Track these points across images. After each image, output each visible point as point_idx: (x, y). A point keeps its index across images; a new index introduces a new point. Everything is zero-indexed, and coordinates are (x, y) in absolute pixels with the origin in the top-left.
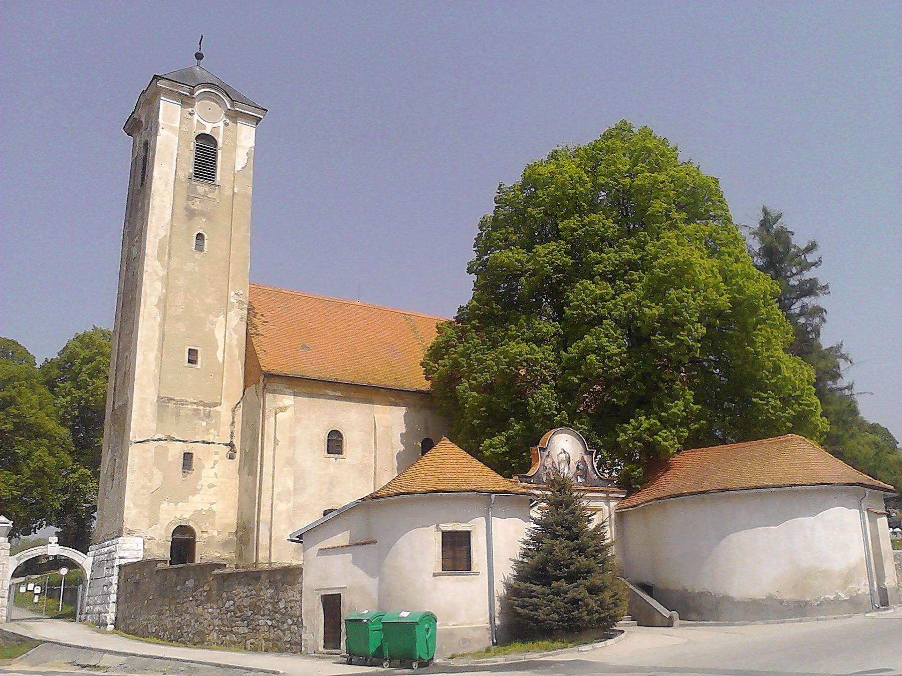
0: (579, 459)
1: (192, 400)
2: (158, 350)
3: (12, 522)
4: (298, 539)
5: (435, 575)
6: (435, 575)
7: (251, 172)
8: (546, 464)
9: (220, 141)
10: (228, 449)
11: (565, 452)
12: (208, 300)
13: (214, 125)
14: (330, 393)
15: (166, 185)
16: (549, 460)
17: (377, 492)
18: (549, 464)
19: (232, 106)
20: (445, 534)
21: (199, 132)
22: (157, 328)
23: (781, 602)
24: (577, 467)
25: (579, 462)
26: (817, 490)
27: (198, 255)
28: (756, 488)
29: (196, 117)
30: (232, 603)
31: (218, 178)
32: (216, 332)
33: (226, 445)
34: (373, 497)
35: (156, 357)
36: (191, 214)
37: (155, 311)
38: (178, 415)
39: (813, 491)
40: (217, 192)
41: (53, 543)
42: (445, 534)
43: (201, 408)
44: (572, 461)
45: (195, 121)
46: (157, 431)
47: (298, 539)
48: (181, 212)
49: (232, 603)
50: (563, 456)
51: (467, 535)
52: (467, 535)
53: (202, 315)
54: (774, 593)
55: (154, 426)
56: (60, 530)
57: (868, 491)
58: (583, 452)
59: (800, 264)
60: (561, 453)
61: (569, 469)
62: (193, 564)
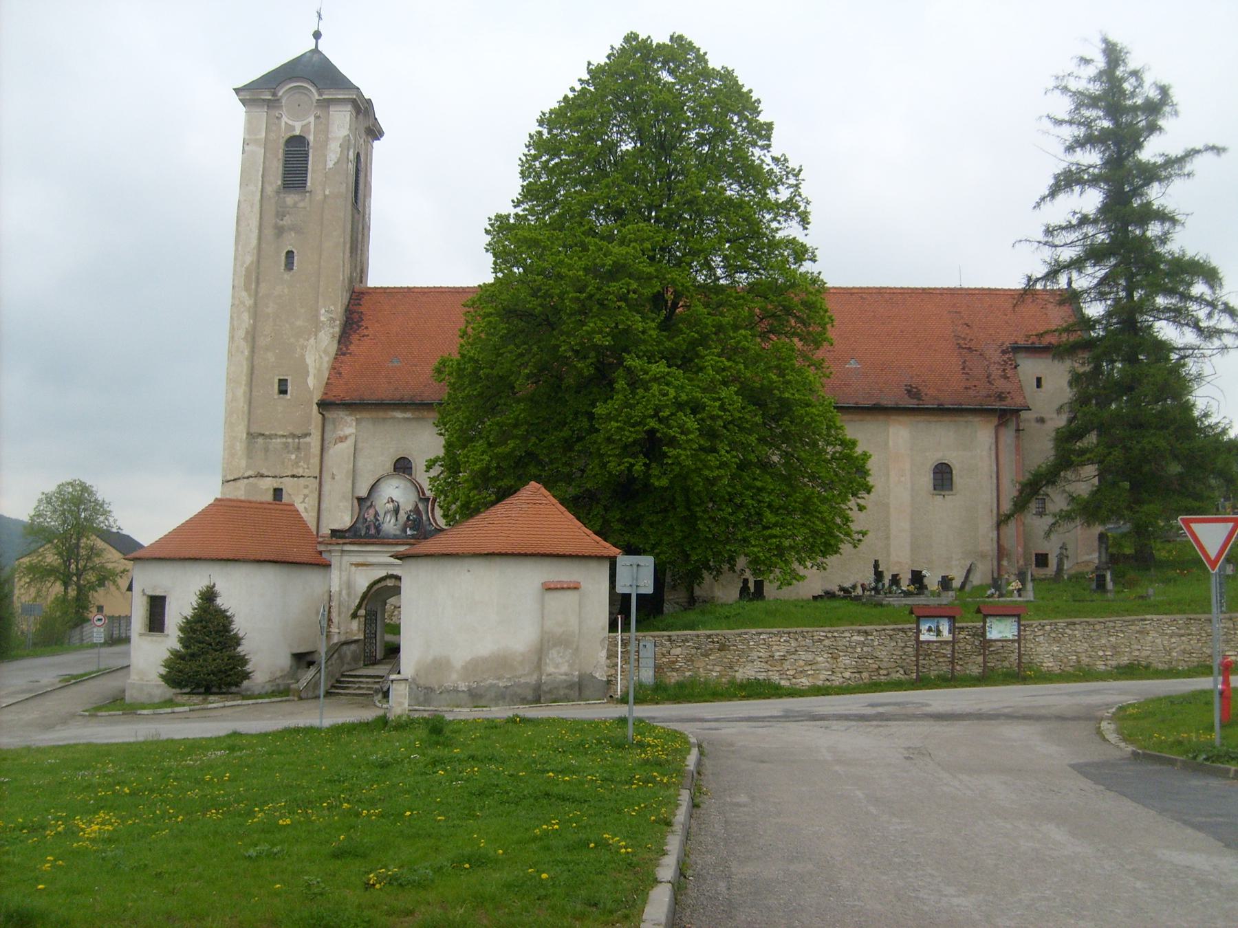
0: (410, 507)
8: (366, 516)
9: (311, 138)
11: (393, 501)
12: (299, 323)
13: (304, 123)
19: (320, 95)
21: (287, 136)
22: (245, 363)
24: (408, 518)
25: (410, 511)
27: (287, 276)
29: (284, 119)
32: (307, 357)
35: (244, 392)
36: (280, 231)
40: (307, 200)
43: (290, 440)
45: (283, 124)
46: (248, 467)
48: (269, 232)
50: (390, 506)
53: (292, 340)
55: (243, 463)
58: (417, 500)
60: (388, 502)
61: (397, 520)
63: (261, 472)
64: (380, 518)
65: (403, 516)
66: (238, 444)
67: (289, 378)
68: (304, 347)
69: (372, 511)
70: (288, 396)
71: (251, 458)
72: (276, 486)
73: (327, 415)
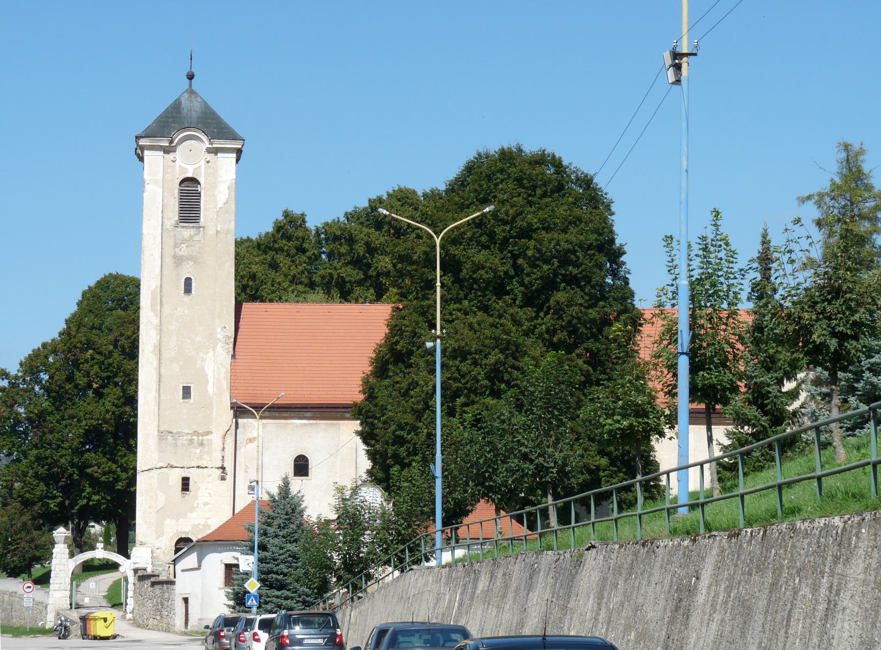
1: (187, 431)
38: (176, 445)
43: (195, 438)
55: (156, 456)
63: (171, 464)
67: (192, 386)
68: (203, 360)
70: (192, 401)
71: (162, 452)
72: (184, 475)
73: (240, 420)
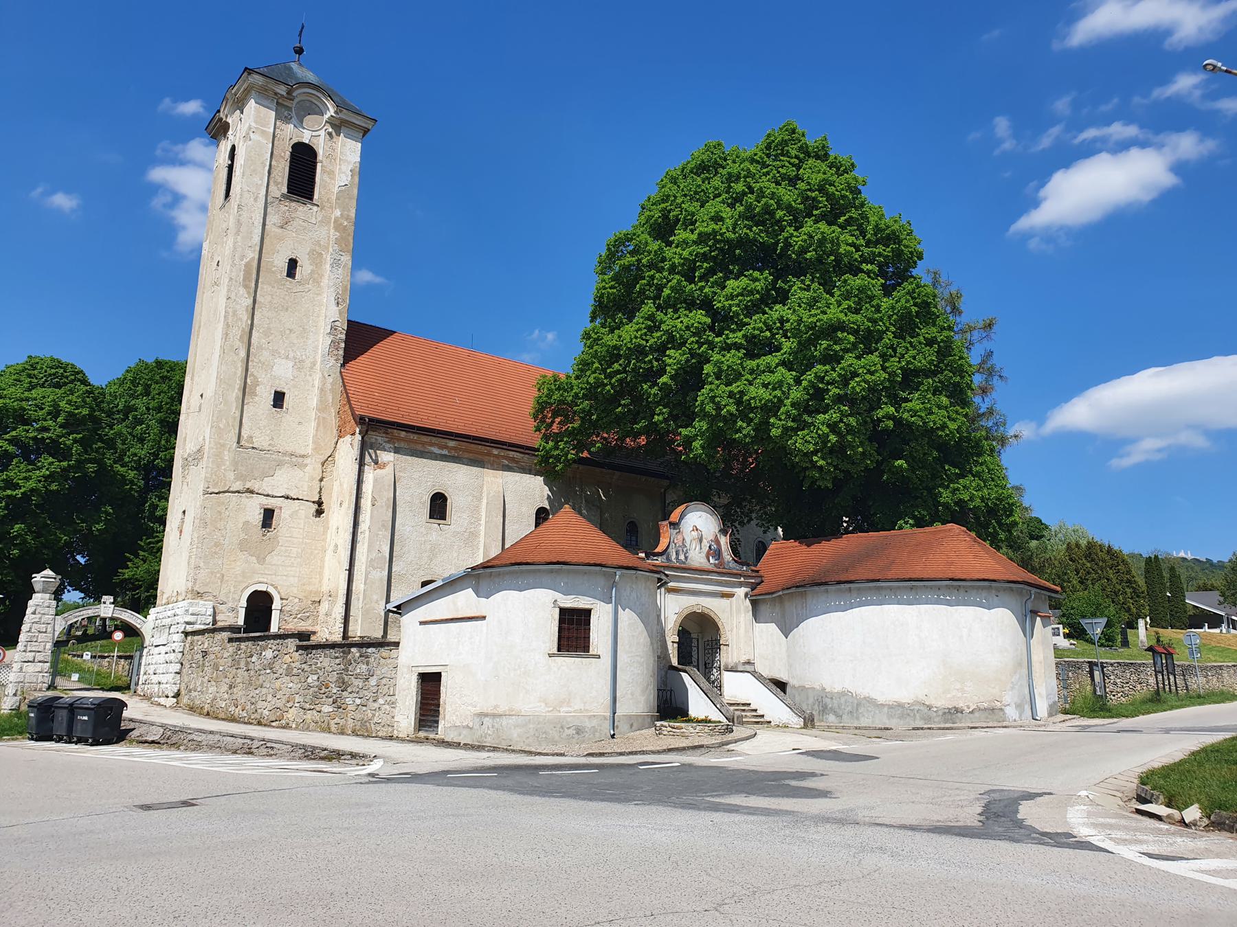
0: (712, 537)
2: (239, 389)
3: (60, 577)
4: (395, 610)
5: (550, 656)
6: (550, 656)
7: (356, 191)
8: (676, 541)
10: (316, 506)
14: (436, 450)
15: (255, 200)
16: (679, 537)
17: (488, 561)
18: (1198, 93)
20: (563, 611)
22: (239, 364)
23: (930, 707)
24: (710, 547)
25: (712, 541)
26: (979, 587)
28: (910, 580)
30: (315, 677)
31: (316, 197)
33: (314, 502)
34: (484, 566)
37: (238, 344)
39: (973, 587)
41: (108, 603)
42: (563, 611)
44: (704, 541)
47: (395, 610)
49: (315, 677)
51: (587, 613)
52: (587, 613)
54: (921, 697)
56: (997, 152)
57: (1034, 590)
59: (577, 733)
62: (266, 633)
64: (687, 544)
65: (706, 544)
66: (226, 453)
69: (679, 537)
